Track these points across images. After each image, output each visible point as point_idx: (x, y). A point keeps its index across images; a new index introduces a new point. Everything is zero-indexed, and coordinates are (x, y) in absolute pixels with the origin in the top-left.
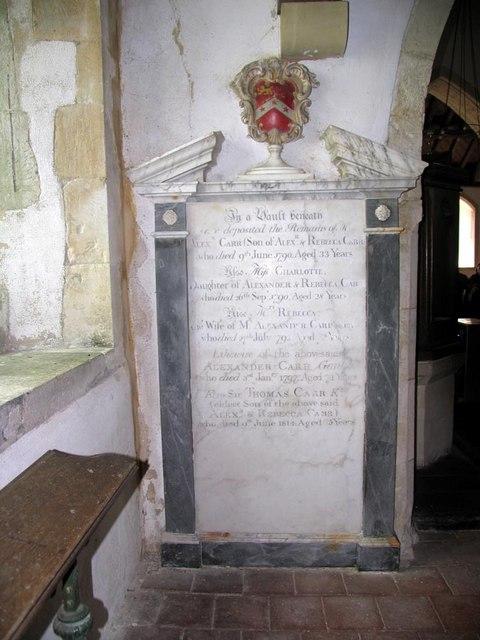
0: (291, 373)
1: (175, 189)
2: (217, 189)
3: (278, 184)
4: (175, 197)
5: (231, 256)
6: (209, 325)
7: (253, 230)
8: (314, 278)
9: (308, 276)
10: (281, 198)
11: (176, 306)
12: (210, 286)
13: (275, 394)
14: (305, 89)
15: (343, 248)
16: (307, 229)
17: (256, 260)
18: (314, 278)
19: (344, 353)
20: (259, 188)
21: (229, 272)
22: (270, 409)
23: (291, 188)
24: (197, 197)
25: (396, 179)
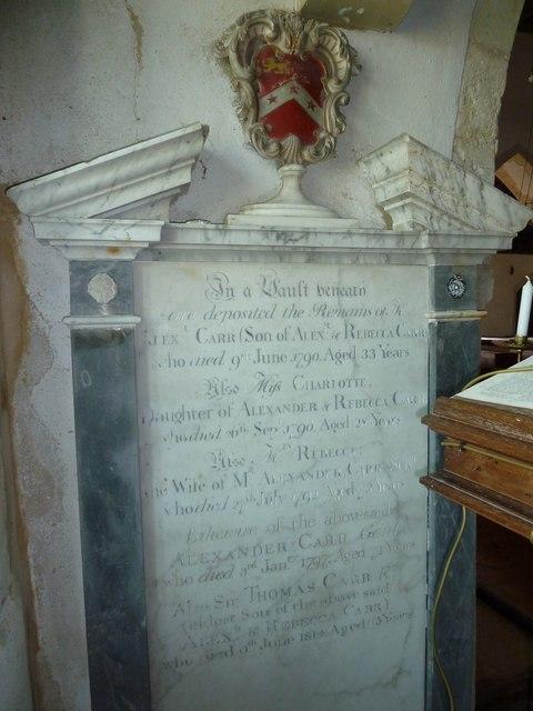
0: (318, 552)
1: (117, 233)
2: (198, 238)
3: (306, 233)
4: (114, 250)
5: (217, 361)
6: (179, 487)
7: (255, 314)
8: (354, 393)
9: (344, 391)
10: (302, 259)
11: (117, 458)
12: (180, 416)
13: (236, 554)
14: (342, 74)
15: (396, 343)
16: (343, 313)
17: (261, 367)
18: (354, 393)
19: (398, 509)
20: (272, 240)
21: (214, 389)
22: (284, 617)
23: (327, 242)
24: (153, 252)
25: (487, 235)
